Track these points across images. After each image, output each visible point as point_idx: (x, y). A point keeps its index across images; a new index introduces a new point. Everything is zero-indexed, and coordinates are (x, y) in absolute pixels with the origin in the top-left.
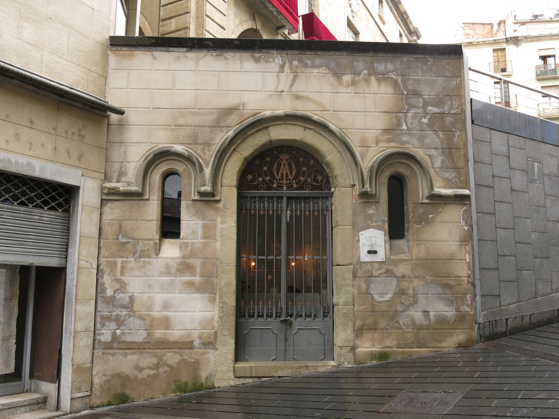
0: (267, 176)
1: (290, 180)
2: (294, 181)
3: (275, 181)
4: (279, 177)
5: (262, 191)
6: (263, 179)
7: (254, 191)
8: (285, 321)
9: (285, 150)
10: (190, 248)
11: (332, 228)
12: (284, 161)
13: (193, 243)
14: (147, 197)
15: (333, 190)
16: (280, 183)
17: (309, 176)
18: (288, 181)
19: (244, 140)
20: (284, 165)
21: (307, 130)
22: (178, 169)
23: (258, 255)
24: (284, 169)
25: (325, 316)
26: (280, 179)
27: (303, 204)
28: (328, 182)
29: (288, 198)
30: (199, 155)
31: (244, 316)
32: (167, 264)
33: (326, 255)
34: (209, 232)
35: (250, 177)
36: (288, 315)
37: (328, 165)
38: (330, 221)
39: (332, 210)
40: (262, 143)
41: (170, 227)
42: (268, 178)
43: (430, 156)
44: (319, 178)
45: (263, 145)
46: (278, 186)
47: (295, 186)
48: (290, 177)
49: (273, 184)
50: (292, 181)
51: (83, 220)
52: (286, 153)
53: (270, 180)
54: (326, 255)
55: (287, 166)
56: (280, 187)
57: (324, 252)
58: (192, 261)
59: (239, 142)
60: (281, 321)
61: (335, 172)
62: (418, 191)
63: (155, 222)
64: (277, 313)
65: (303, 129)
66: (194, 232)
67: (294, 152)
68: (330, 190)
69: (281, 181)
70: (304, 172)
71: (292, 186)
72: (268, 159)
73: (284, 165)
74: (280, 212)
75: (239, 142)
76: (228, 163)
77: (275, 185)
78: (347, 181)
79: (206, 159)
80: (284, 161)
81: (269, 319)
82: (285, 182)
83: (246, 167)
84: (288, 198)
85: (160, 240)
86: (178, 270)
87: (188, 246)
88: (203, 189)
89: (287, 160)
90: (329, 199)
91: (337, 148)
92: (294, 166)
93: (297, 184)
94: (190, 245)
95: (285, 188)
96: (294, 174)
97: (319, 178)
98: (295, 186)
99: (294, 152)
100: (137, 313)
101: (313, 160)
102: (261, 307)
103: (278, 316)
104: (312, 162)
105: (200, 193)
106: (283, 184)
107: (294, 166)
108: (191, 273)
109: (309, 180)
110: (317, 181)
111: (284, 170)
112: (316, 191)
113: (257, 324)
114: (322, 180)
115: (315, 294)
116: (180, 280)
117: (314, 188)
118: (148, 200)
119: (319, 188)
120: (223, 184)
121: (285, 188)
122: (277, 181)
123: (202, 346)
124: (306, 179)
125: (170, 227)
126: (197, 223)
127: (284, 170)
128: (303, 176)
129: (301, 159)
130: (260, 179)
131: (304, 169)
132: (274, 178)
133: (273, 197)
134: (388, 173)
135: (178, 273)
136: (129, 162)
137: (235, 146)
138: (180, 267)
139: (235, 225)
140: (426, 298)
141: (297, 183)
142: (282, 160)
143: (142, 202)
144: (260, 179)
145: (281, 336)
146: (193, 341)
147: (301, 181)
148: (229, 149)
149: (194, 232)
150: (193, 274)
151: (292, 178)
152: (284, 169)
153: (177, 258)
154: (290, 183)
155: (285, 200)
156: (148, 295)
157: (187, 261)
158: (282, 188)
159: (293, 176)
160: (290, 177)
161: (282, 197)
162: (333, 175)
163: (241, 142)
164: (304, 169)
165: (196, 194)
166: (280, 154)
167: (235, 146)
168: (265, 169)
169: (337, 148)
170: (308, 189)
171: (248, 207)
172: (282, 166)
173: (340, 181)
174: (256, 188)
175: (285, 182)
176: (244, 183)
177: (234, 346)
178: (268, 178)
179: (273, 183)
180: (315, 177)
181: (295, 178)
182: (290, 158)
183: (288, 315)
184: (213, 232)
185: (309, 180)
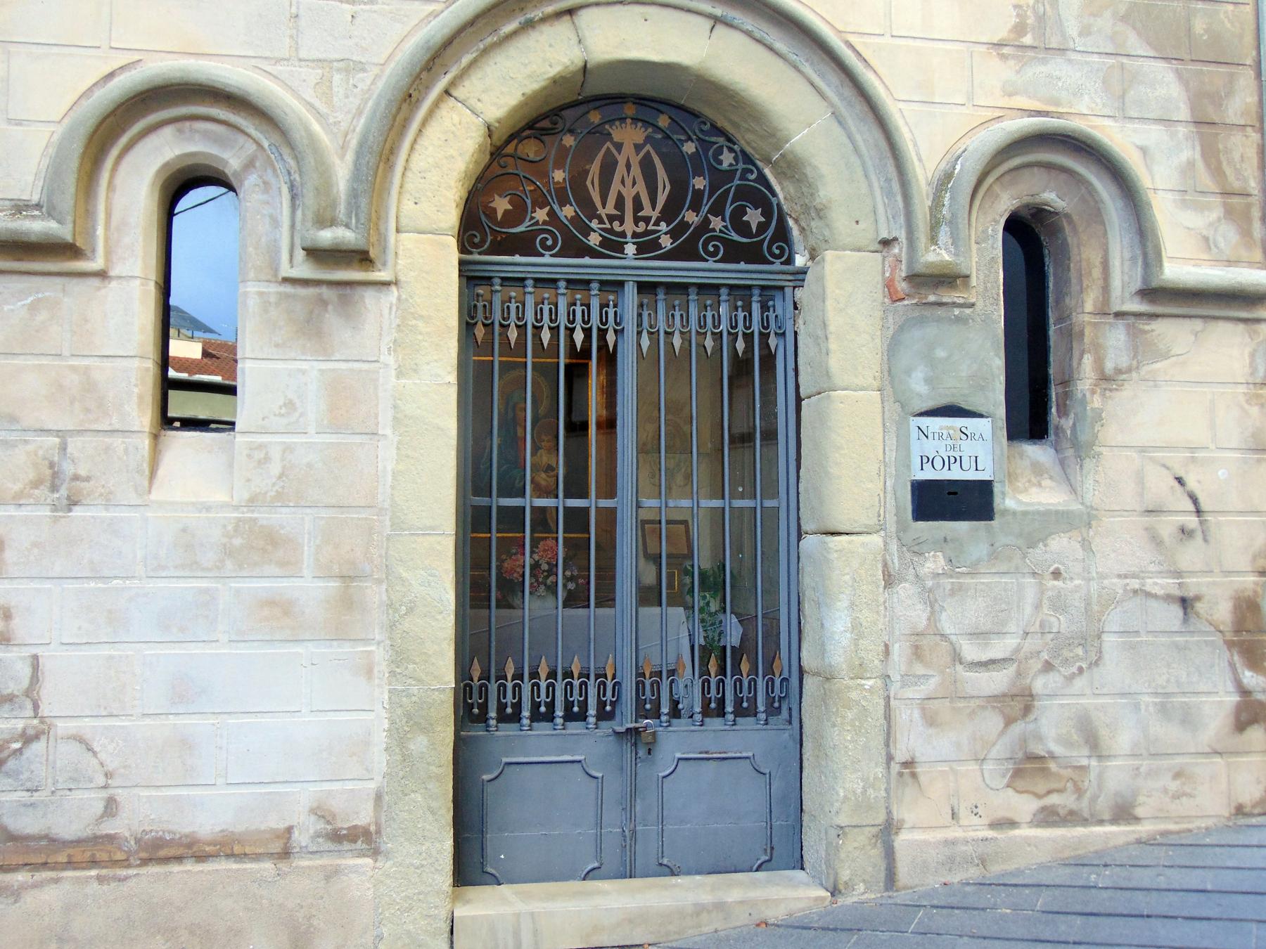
0: (563, 202)
1: (647, 220)
2: (663, 226)
3: (594, 224)
4: (610, 209)
5: (547, 259)
6: (552, 214)
7: (517, 258)
8: (633, 734)
9: (630, 110)
10: (275, 468)
11: (799, 400)
12: (628, 150)
13: (288, 449)
14: (97, 264)
15: (800, 261)
16: (611, 231)
17: (717, 210)
18: (642, 224)
19: (485, 52)
20: (628, 166)
21: (721, 30)
22: (226, 155)
23: (567, 496)
24: (629, 182)
25: (773, 710)
26: (611, 218)
27: (694, 311)
28: (783, 234)
29: (645, 288)
30: (311, 106)
31: (483, 718)
32: (184, 530)
33: (775, 495)
34: (345, 410)
35: (502, 205)
36: (641, 713)
37: (792, 168)
38: (791, 374)
39: (796, 333)
40: (553, 72)
41: (191, 394)
42: (568, 212)
43: (1144, 150)
44: (754, 217)
45: (556, 82)
46: (605, 243)
47: (666, 242)
48: (647, 211)
49: (586, 235)
50: (657, 224)
51: (753, 601)
52: (635, 120)
53: (575, 220)
54: (775, 495)
55: (636, 171)
56: (613, 246)
57: (771, 490)
58: (281, 518)
59: (466, 60)
60: (617, 733)
61: (822, 193)
62: (1099, 273)
63: (136, 363)
64: (601, 705)
65: (708, 24)
66: (290, 405)
67: (663, 121)
68: (790, 261)
69: (616, 224)
70: (698, 194)
71: (655, 245)
72: (569, 141)
73: (628, 166)
74: (611, 338)
75: (466, 60)
76: (424, 141)
77: (594, 240)
78: (862, 225)
79: (337, 123)
80: (628, 150)
81: (575, 727)
82: (629, 227)
83: (487, 167)
84: (645, 288)
85: (156, 437)
86: (228, 552)
87: (267, 459)
88: (327, 236)
89: (638, 148)
90: (788, 291)
91: (832, 105)
92: (662, 175)
93: (674, 239)
94: (276, 454)
95: (630, 249)
96: (662, 199)
97: (754, 217)
98: (666, 242)
99: (663, 121)
100: (60, 724)
101: (731, 150)
102: (543, 685)
103: (603, 715)
104: (727, 159)
105: (316, 254)
106: (623, 234)
107: (662, 175)
108: (283, 564)
109: (717, 223)
110: (743, 228)
111: (629, 184)
112: (742, 266)
113: (536, 743)
114: (762, 227)
115: (671, 610)
116: (238, 591)
117: (734, 253)
118: (102, 275)
119: (752, 254)
120: (403, 221)
121: (630, 249)
122: (601, 222)
123: (330, 846)
124: (706, 221)
125: (191, 394)
126: (304, 372)
127: (629, 184)
128: (696, 207)
129: (689, 148)
130: (541, 215)
131: (699, 183)
132: (593, 215)
133: (588, 282)
134: (1006, 203)
135: (229, 564)
136: (19, 123)
137: (449, 77)
138: (237, 542)
139: (453, 378)
140: (1132, 647)
141: (674, 234)
142: (619, 147)
143: (76, 286)
144: (541, 215)
145: (614, 787)
146: (289, 830)
147: (688, 225)
148: (428, 88)
149: (290, 405)
150: (290, 567)
151: (655, 215)
152: (629, 182)
153: (223, 506)
154: (647, 233)
155: (630, 292)
156: (106, 651)
157: (265, 517)
158: (619, 248)
159: (659, 206)
160: (647, 211)
161: (621, 284)
162: (806, 209)
163: (473, 64)
164: (699, 183)
165: (300, 255)
166: (611, 122)
167: (449, 77)
168: (559, 176)
169: (832, 105)
170: (713, 255)
171: (497, 317)
172: (621, 169)
173: (841, 222)
174: (525, 245)
175: (629, 227)
176: (482, 229)
177: (449, 844)
178: (568, 212)
179: (587, 231)
180: (741, 211)
181: (669, 213)
182: (648, 139)
183: (641, 713)
184: (378, 411)
185: (717, 223)
